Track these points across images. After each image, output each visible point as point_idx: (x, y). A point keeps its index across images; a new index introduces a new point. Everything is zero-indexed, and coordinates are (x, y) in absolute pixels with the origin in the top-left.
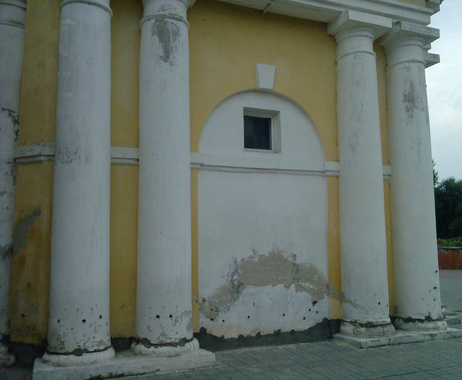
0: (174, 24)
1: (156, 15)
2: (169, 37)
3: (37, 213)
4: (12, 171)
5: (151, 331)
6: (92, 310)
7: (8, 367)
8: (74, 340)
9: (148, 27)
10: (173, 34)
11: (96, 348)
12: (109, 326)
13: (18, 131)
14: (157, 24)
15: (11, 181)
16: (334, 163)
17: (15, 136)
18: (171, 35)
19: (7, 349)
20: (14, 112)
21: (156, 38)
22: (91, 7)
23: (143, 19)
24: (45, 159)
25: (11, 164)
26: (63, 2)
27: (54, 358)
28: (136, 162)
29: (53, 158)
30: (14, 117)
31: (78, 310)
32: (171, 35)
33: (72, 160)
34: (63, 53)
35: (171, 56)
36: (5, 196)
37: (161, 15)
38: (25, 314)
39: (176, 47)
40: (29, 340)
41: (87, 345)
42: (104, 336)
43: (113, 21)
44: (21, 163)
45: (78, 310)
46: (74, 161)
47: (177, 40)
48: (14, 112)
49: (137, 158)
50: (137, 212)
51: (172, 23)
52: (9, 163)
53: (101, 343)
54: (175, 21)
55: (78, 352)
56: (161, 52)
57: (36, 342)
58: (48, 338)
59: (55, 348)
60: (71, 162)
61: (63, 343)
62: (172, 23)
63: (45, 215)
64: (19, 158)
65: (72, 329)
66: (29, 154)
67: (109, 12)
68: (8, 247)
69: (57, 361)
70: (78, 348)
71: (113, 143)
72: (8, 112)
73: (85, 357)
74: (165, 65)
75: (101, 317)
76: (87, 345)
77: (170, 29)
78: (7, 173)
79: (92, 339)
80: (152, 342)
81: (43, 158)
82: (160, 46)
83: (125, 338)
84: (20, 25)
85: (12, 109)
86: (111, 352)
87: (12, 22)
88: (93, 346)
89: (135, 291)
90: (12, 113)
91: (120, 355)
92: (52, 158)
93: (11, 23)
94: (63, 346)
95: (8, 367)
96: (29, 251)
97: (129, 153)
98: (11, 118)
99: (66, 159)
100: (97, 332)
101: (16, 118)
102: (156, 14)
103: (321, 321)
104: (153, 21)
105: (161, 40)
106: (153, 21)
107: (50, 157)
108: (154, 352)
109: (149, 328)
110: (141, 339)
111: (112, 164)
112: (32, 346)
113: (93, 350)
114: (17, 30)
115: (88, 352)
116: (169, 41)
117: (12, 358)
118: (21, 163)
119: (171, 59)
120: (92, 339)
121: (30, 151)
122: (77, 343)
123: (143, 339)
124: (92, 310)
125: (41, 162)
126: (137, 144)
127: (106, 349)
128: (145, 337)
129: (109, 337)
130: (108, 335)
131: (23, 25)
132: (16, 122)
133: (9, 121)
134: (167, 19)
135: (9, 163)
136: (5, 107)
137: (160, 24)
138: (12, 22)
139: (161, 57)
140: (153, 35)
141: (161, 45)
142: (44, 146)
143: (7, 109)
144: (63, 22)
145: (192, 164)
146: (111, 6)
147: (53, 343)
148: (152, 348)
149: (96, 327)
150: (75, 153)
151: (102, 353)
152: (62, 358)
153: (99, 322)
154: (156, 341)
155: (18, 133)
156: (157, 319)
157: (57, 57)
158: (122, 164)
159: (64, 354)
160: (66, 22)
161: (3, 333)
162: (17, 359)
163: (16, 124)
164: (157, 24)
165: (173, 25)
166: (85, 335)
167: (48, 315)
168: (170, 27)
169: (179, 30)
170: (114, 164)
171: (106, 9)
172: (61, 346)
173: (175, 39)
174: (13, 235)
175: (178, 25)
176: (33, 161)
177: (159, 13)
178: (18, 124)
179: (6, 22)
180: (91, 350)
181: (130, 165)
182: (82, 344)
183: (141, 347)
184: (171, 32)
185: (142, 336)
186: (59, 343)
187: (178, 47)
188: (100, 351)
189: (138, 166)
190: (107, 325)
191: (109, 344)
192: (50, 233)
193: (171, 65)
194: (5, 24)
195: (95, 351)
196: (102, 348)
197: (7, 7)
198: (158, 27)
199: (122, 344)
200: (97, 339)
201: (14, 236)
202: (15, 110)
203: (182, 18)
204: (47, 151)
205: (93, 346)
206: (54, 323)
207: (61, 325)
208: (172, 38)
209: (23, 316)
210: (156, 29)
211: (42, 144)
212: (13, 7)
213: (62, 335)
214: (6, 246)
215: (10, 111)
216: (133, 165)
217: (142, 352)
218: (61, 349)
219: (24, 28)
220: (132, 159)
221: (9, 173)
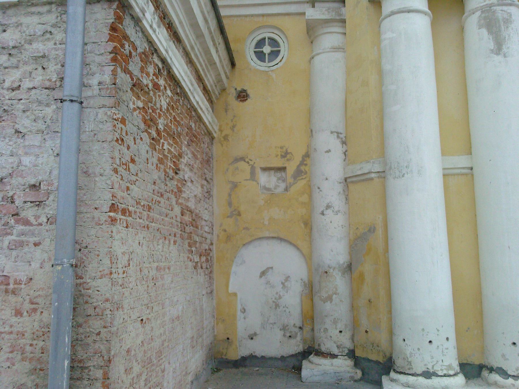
0: (504, 11)
1: (481, 7)
2: (500, 26)
3: (372, 230)
4: (344, 190)
5: (508, 359)
6: (438, 330)
7: (355, 381)
8: (422, 362)
9: (472, 22)
10: (504, 22)
11: (445, 372)
12: (456, 350)
13: (346, 151)
14: (483, 15)
15: (344, 200)
16: (466, 156)
17: (344, 157)
18: (502, 23)
19: (353, 363)
20: (341, 134)
21: (484, 31)
22: (411, 15)
23: (464, 15)
24: (376, 176)
25: (342, 184)
26: (382, 17)
27: (402, 378)
28: (469, 171)
29: (382, 175)
30: (342, 138)
31: (423, 330)
32: (502, 23)
33: (404, 174)
34: (387, 67)
35: (504, 47)
36: (339, 214)
37: (487, 5)
38: (368, 330)
39: (509, 36)
40: (373, 357)
41: (436, 368)
42: (452, 360)
43: (434, 24)
44: (352, 182)
45: (423, 330)
46: (406, 175)
47: (510, 28)
48: (341, 134)
49: (470, 166)
50: (476, 225)
51: (502, 10)
52: (340, 183)
53: (450, 367)
54: (505, 8)
55: (428, 375)
56: (492, 45)
57: (381, 359)
58: (393, 356)
59: (402, 367)
60: (403, 176)
61: (410, 363)
62: (502, 10)
63: (380, 232)
64: (349, 177)
65: (419, 349)
66: (359, 172)
67: (429, 15)
68: (346, 264)
69: (406, 381)
70: (426, 370)
71: (444, 153)
72: (336, 134)
73: (435, 381)
74: (498, 59)
75: (447, 339)
76: (435, 368)
77: (500, 18)
78: (340, 193)
79: (440, 363)
80: (509, 373)
81: (373, 175)
82: (490, 39)
83: (474, 364)
84: (342, 50)
85: (340, 131)
86: (460, 379)
87: (334, 48)
88: (442, 370)
89: (481, 313)
90: (340, 135)
91: (469, 382)
92: (382, 175)
93: (333, 50)
94: (411, 367)
95: (355, 381)
96: (367, 268)
97: (461, 162)
98: (339, 140)
99: (398, 173)
100: (445, 355)
101: (344, 139)
102: (482, 5)
103: (234, 269)
104: (478, 13)
105: (490, 32)
106: (478, 13)
107: (380, 174)
108: (514, 385)
109: (503, 356)
110: (495, 368)
111: (444, 175)
112: (377, 363)
113: (442, 374)
114: (339, 55)
115: (438, 376)
116: (500, 31)
117: (359, 374)
118: (352, 182)
119: (505, 49)
120: (440, 363)
121: (360, 169)
122: (425, 365)
123: (498, 367)
124: (438, 330)
125: (372, 179)
126: (469, 152)
127: (455, 375)
128: (499, 366)
129: (457, 363)
130: (456, 359)
131: (344, 49)
132: (344, 143)
133: (338, 142)
134: (495, 8)
135: (340, 183)
136: (334, 130)
137: (487, 15)
138: (334, 48)
139: (492, 51)
140: (479, 29)
141: (491, 38)
142: (374, 163)
143: (335, 132)
144: (383, 37)
145: (444, 169)
146: (430, 9)
147: (399, 363)
148: (510, 381)
149: (444, 350)
150: (406, 167)
151: (452, 378)
152: (411, 379)
153: (447, 344)
154: (514, 372)
155: (346, 153)
156: (513, 347)
157: (380, 73)
158: (454, 175)
159: (413, 375)
160: (387, 36)
161: (348, 347)
162: (363, 374)
163: (344, 145)
164: (483, 15)
165: (503, 12)
166: (432, 358)
167: (391, 333)
168: (500, 15)
169: (511, 16)
170: (447, 175)
171: (425, 13)
172: (409, 366)
173: (507, 27)
174: (349, 253)
175: (509, 11)
176: (364, 178)
177: (485, 3)
178: (346, 145)
179: (329, 50)
180: (440, 373)
181: (462, 174)
182: (430, 367)
183: (495, 377)
184: (501, 20)
185: (495, 364)
186: (406, 363)
187: (512, 35)
188: (450, 376)
189: (472, 175)
190: (455, 348)
191: (458, 369)
192: (386, 250)
193: (505, 56)
194: (329, 52)
195: (445, 376)
196: (451, 372)
197: (327, 35)
198: (485, 18)
199: (472, 370)
200: (446, 363)
201: (351, 254)
202: (342, 132)
203: (514, 1)
204: (377, 168)
205: (442, 370)
206: (398, 341)
207: (406, 344)
208: (503, 27)
209: (366, 332)
210: (482, 22)
211: (372, 161)
212: (334, 34)
213: (408, 356)
214: (344, 263)
215: (338, 133)
216: (466, 174)
217: (498, 383)
218: (409, 369)
219: (345, 52)
220: (464, 168)
221: (342, 192)
